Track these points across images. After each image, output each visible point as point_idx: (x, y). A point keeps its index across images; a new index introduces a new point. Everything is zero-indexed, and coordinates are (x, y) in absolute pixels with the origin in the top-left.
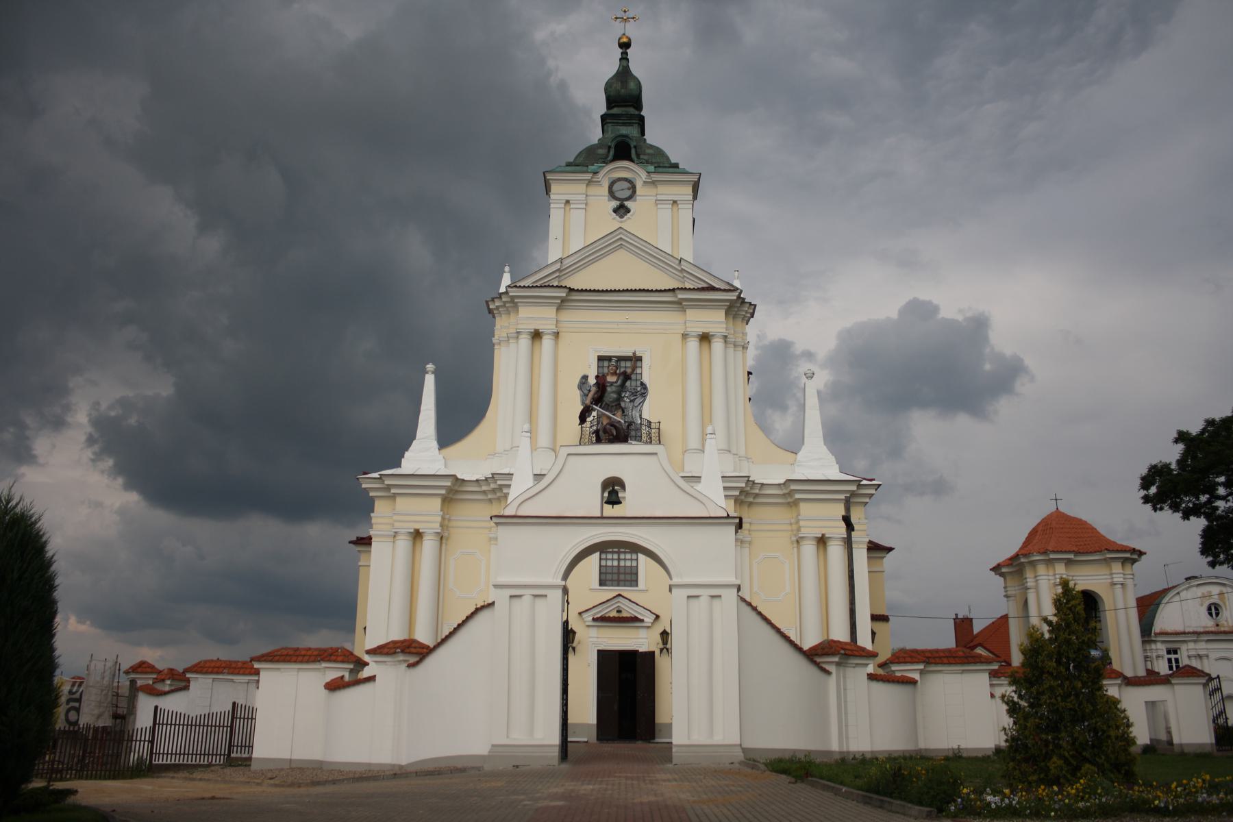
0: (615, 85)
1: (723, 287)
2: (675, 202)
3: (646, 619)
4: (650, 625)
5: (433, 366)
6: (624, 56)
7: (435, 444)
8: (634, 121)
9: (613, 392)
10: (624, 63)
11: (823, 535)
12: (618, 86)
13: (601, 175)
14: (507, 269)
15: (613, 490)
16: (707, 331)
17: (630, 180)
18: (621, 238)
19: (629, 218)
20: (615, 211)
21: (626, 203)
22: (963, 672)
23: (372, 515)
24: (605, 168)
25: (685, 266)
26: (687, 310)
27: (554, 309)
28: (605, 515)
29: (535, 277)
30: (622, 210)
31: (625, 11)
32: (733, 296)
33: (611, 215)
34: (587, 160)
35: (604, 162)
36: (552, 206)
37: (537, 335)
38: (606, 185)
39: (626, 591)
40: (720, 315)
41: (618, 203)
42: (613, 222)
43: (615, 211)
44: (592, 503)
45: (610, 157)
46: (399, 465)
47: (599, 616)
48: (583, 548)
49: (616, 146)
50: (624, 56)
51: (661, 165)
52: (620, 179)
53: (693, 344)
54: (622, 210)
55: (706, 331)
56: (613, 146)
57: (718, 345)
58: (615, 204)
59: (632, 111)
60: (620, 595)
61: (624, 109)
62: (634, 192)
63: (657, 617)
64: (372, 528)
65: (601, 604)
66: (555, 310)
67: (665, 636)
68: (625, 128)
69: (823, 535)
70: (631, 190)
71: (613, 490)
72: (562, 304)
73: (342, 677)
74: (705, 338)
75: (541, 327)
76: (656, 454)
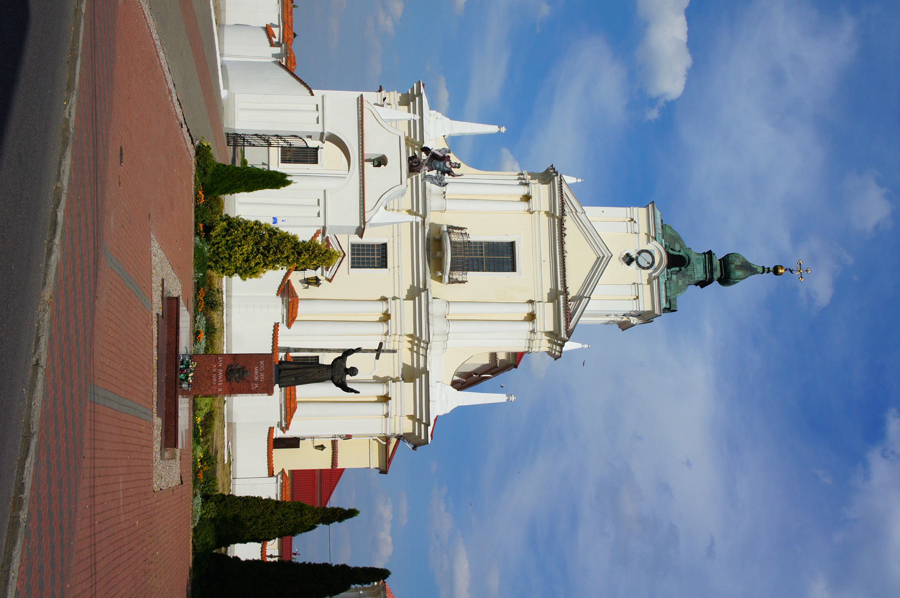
0: (737, 260)
1: (571, 327)
2: (638, 298)
3: (328, 272)
4: (325, 275)
5: (504, 132)
6: (766, 270)
7: (447, 134)
8: (708, 275)
9: (440, 165)
10: (760, 270)
11: (390, 399)
12: (738, 263)
13: (655, 242)
14: (579, 180)
15: (380, 162)
16: (537, 317)
17: (653, 266)
18: (604, 256)
19: (622, 264)
20: (628, 255)
21: (634, 262)
22: (281, 405)
23: (396, 92)
24: (661, 246)
25: (584, 301)
26: (552, 304)
27: (548, 210)
28: (366, 163)
29: (571, 196)
30: (629, 259)
31: (807, 271)
32: (563, 335)
33: (624, 252)
34: (670, 238)
35: (666, 246)
36: (628, 209)
37: (527, 198)
38: (649, 247)
39: (347, 261)
40: (550, 328)
41: (634, 257)
42: (618, 252)
43: (628, 255)
44: (371, 150)
45: (671, 252)
46: (431, 109)
47: (330, 241)
48: (346, 143)
49: (681, 256)
50: (766, 270)
51: (668, 290)
52: (653, 258)
53: (528, 309)
54: (629, 259)
55: (537, 316)
56: (681, 254)
57: (528, 326)
58: (634, 255)
59: (717, 274)
60: (344, 255)
61: (719, 268)
62: (644, 268)
63: (330, 281)
64: (386, 92)
65: (338, 242)
66: (547, 210)
67: (314, 281)
68: (702, 268)
69: (390, 399)
70: (649, 265)
71: (380, 162)
72: (550, 214)
73: (275, 37)
74: (531, 317)
75: (533, 200)
76: (401, 184)
